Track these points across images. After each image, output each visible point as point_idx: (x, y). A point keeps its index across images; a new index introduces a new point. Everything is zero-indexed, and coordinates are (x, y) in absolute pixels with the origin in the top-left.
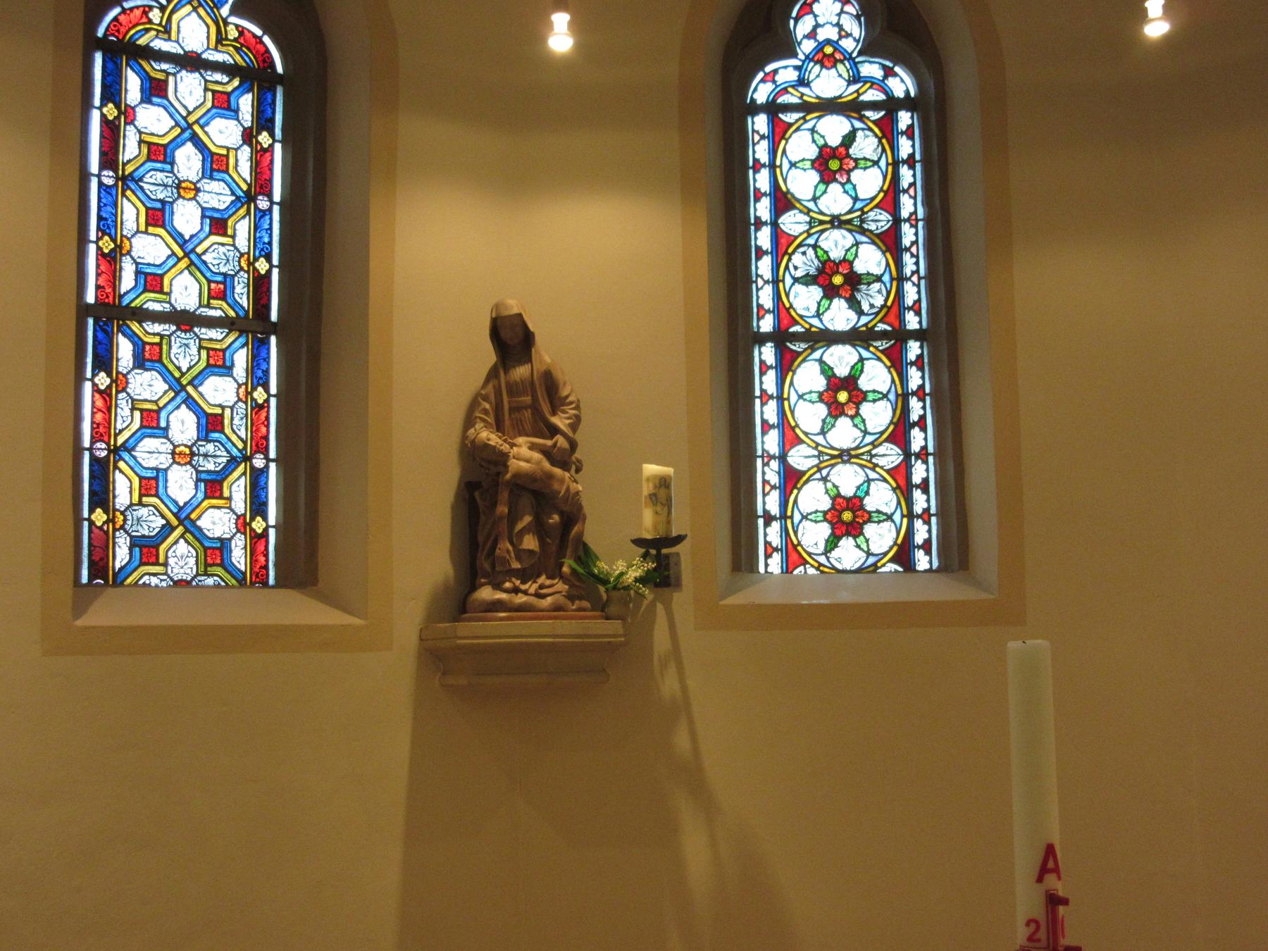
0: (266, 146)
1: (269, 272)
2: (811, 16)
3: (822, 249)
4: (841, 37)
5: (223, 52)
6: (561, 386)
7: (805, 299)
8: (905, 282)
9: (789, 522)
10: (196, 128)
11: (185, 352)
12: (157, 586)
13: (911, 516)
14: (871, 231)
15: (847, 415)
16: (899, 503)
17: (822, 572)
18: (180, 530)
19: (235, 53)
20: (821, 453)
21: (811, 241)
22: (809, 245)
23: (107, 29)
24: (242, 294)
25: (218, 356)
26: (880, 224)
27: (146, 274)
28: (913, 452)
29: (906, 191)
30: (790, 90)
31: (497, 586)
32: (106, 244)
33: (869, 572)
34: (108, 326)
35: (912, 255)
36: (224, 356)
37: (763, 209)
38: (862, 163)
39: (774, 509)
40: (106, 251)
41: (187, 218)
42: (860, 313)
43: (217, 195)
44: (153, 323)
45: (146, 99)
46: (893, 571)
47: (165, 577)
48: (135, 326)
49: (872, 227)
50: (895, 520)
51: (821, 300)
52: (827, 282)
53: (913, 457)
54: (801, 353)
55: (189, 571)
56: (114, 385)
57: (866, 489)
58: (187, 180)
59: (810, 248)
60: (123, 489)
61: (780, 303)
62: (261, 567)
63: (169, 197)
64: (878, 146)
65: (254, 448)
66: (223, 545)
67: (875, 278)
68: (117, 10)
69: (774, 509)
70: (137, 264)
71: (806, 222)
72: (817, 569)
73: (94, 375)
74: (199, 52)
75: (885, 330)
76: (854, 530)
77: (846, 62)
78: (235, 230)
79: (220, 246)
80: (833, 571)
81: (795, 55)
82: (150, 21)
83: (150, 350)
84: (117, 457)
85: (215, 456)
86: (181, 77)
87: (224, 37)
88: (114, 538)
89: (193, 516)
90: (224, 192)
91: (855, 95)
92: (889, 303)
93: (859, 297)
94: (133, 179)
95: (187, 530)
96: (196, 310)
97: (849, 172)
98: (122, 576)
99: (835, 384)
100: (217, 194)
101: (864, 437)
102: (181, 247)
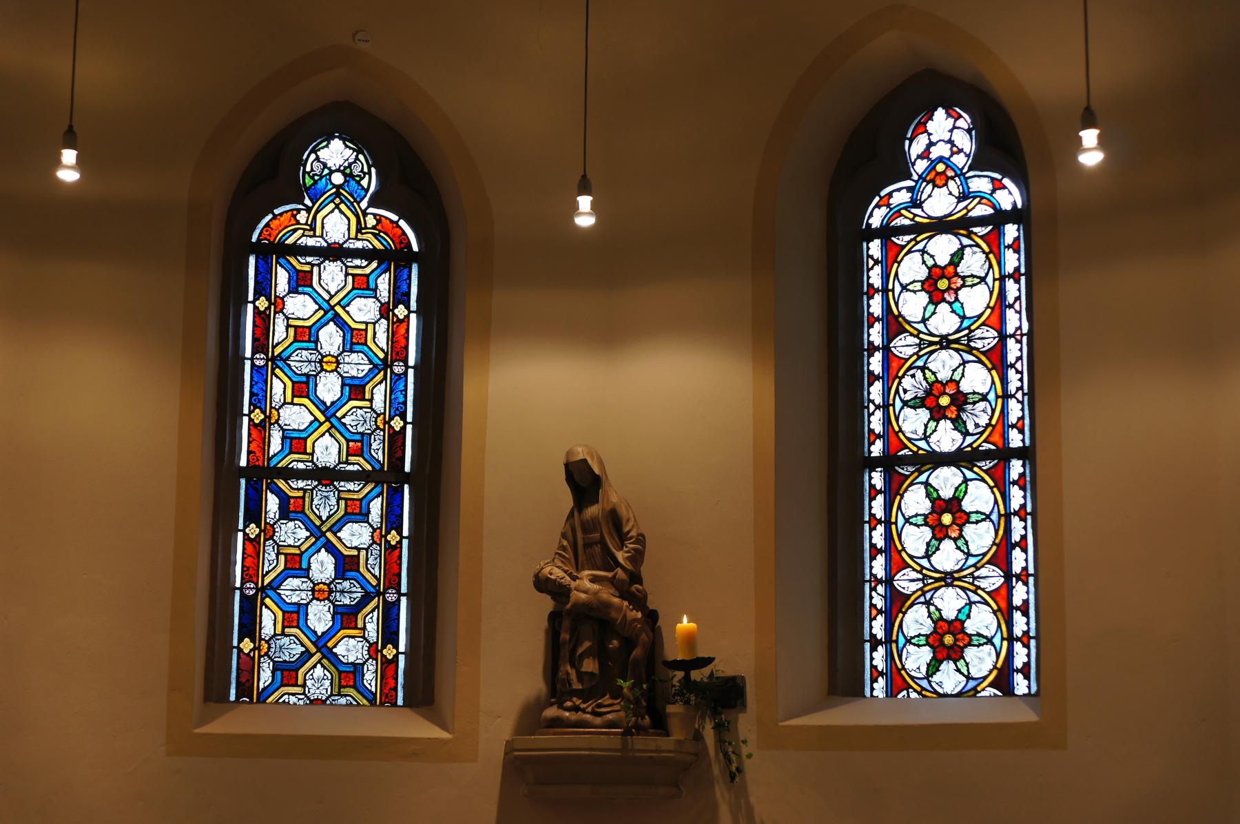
0: (401, 317)
1: (404, 429)
2: (926, 134)
3: (930, 370)
4: (953, 154)
5: (363, 240)
6: (624, 522)
7: (913, 422)
8: (1009, 399)
9: (894, 645)
10: (338, 309)
11: (325, 503)
12: (295, 704)
13: (1011, 639)
14: (977, 349)
15: (950, 538)
16: (999, 626)
17: (924, 696)
18: (318, 656)
19: (373, 238)
20: (925, 575)
21: (920, 363)
22: (918, 368)
23: (260, 235)
24: (378, 450)
25: (355, 505)
26: (986, 341)
27: (292, 439)
28: (1014, 573)
29: (1011, 306)
30: (903, 212)
31: (561, 707)
32: (257, 416)
33: (968, 696)
34: (257, 484)
35: (1017, 372)
36: (361, 504)
37: (876, 335)
38: (969, 281)
39: (879, 633)
40: (257, 421)
41: (329, 388)
42: (966, 434)
43: (356, 366)
44: (297, 480)
45: (293, 290)
46: (992, 695)
47: (303, 697)
48: (281, 484)
49: (979, 344)
50: (995, 643)
51: (928, 422)
52: (934, 404)
53: (1014, 579)
54: (909, 476)
55: (324, 692)
56: (262, 534)
57: (967, 612)
58: (330, 355)
59: (919, 371)
60: (268, 621)
61: (890, 427)
62: (390, 689)
63: (313, 371)
64: (985, 261)
65: (387, 585)
66: (357, 669)
67: (980, 397)
68: (270, 216)
69: (879, 633)
70: (284, 430)
71: (916, 345)
72: (919, 693)
73: (246, 526)
74: (341, 242)
75: (990, 450)
76: (955, 654)
77: (957, 179)
78: (372, 394)
79: (358, 410)
80: (935, 696)
81: (909, 177)
82: (298, 223)
83: (294, 503)
84: (264, 595)
85: (351, 592)
86: (325, 266)
87: (363, 226)
88: (259, 662)
89: (330, 644)
90: (362, 362)
91: (965, 211)
92: (994, 422)
93: (965, 418)
94: (282, 359)
95: (324, 657)
96: (336, 466)
97: (956, 291)
98: (265, 694)
99: (940, 505)
100: (356, 364)
101: (967, 559)
102: (323, 413)
